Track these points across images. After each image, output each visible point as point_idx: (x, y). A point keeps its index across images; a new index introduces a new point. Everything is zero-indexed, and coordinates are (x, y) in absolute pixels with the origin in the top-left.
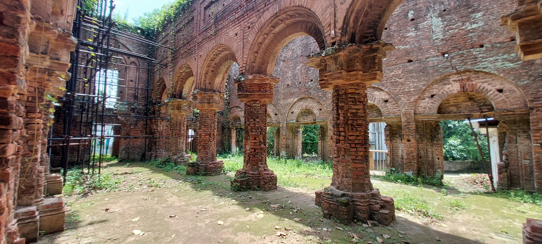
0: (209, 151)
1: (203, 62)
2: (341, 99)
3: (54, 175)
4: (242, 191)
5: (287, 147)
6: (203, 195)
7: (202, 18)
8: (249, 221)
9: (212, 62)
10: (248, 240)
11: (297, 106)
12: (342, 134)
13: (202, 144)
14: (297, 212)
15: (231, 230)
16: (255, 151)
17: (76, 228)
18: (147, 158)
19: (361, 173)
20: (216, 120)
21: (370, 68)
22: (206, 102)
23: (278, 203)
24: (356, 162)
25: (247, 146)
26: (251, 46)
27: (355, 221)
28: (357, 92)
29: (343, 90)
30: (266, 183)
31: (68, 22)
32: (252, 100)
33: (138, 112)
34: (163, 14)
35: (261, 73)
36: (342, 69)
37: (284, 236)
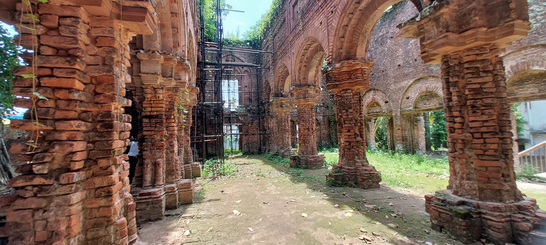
0: (308, 145)
1: (295, 59)
2: (452, 72)
3: (196, 163)
4: (338, 187)
5: (404, 139)
6: (297, 187)
7: (291, 16)
8: (335, 218)
9: (303, 57)
10: (326, 237)
11: (413, 88)
12: (458, 120)
13: (302, 139)
14: (395, 217)
15: (312, 223)
16: (350, 144)
17: (200, 203)
18: (262, 151)
19: (494, 174)
20: (313, 114)
21: (502, 18)
22: (302, 97)
23: (374, 204)
24: (484, 158)
25: (341, 139)
26: (336, 32)
27: (484, 240)
28: (479, 58)
29: (455, 59)
30: (364, 180)
31: (183, 51)
32: (343, 90)
33: (253, 113)
34: (263, 23)
35: (351, 59)
36: (447, 31)
37: (368, 240)
